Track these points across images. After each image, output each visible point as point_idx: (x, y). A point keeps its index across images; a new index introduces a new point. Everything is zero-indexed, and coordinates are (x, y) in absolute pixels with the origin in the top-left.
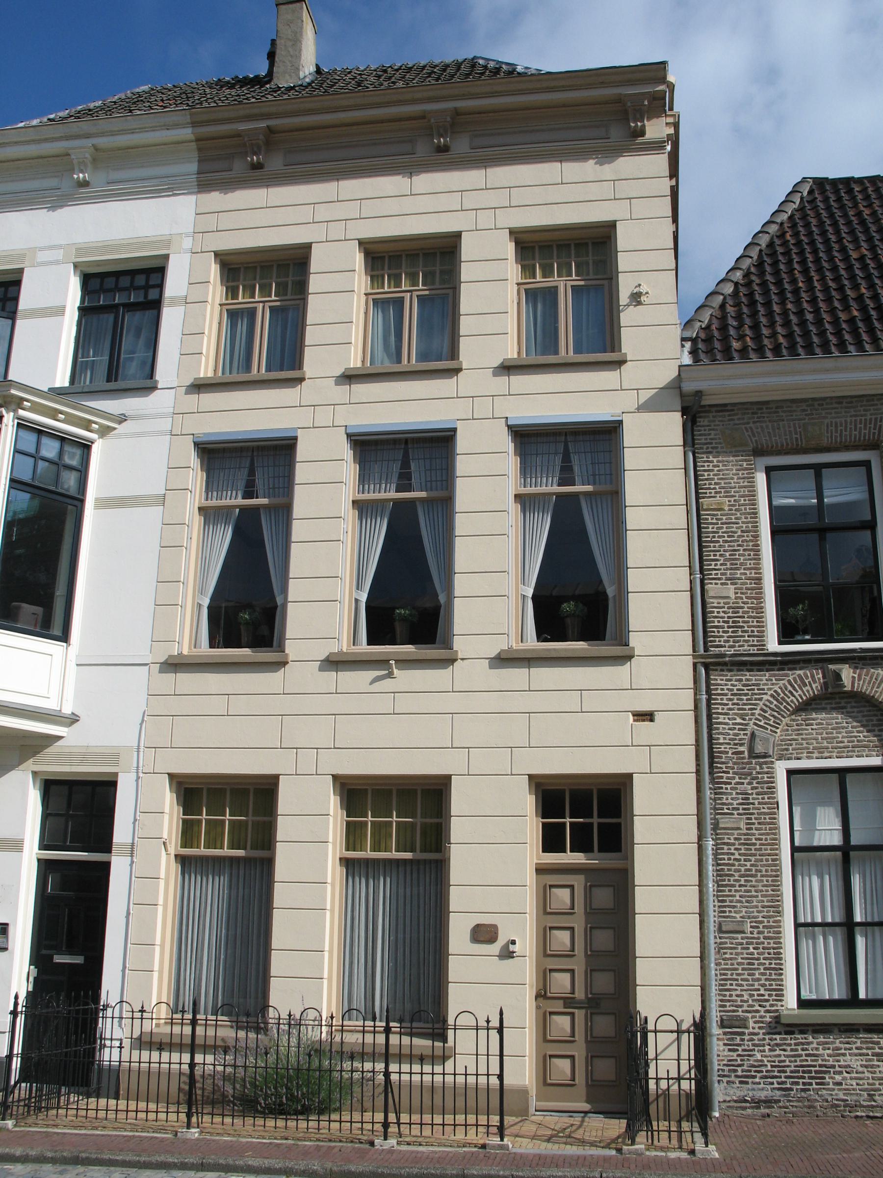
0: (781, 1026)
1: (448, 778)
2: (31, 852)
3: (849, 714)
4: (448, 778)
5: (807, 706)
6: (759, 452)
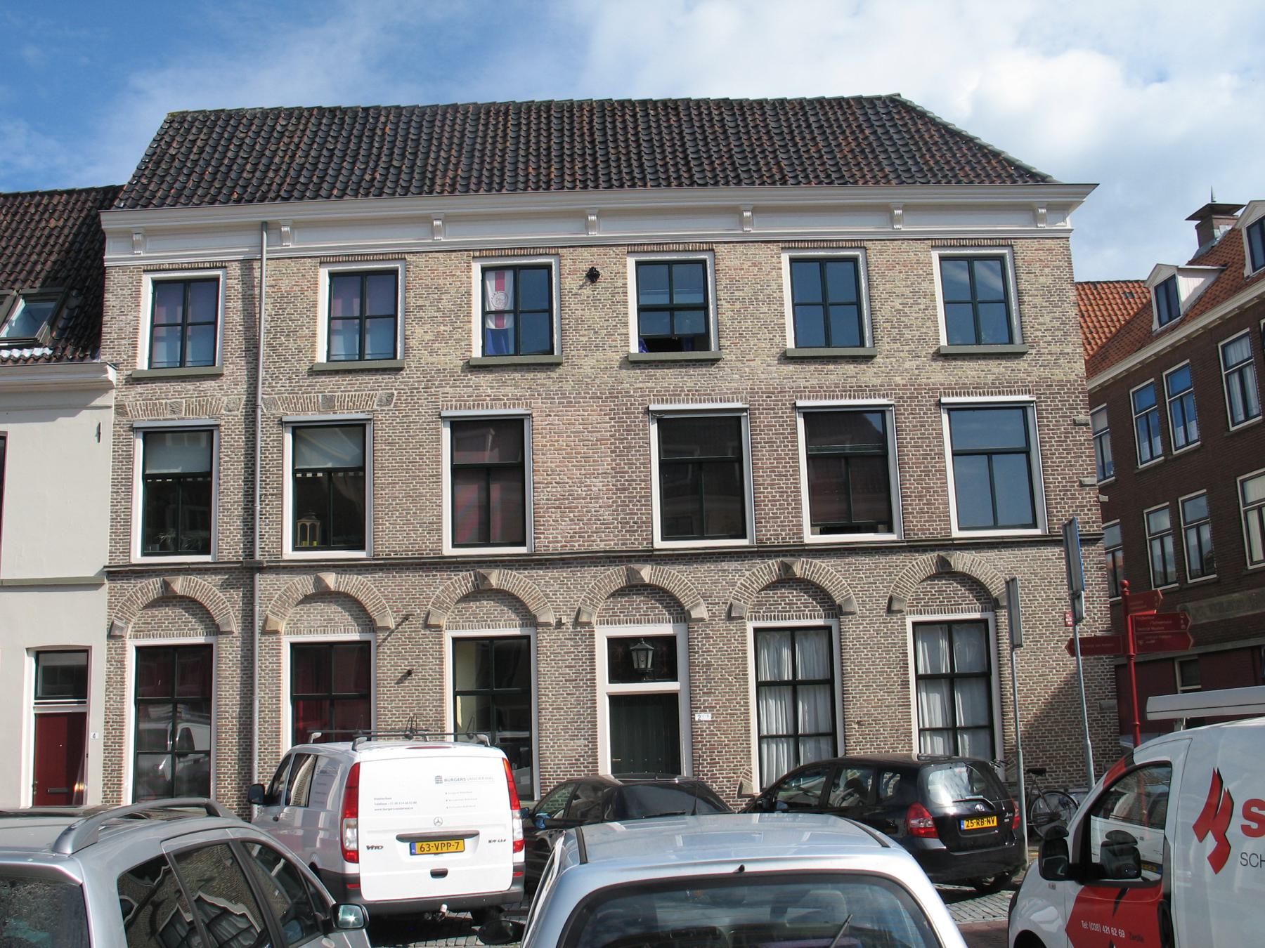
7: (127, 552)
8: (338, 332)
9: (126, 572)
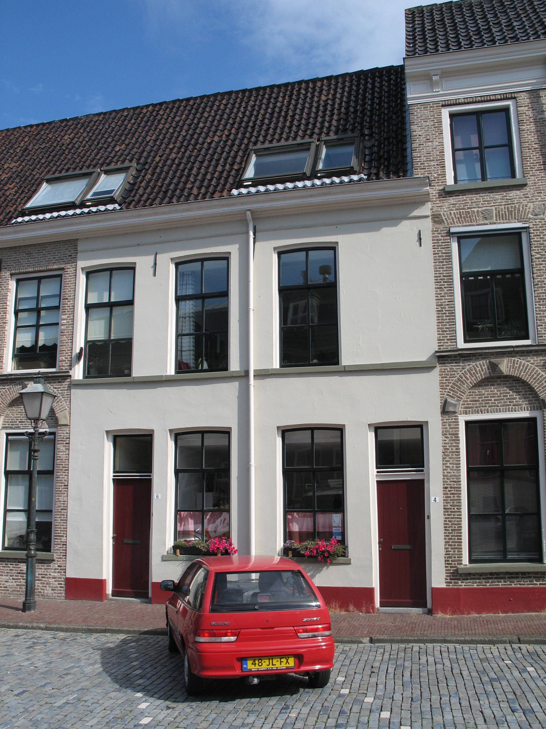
7: (454, 339)
8: (461, 162)
9: (455, 356)
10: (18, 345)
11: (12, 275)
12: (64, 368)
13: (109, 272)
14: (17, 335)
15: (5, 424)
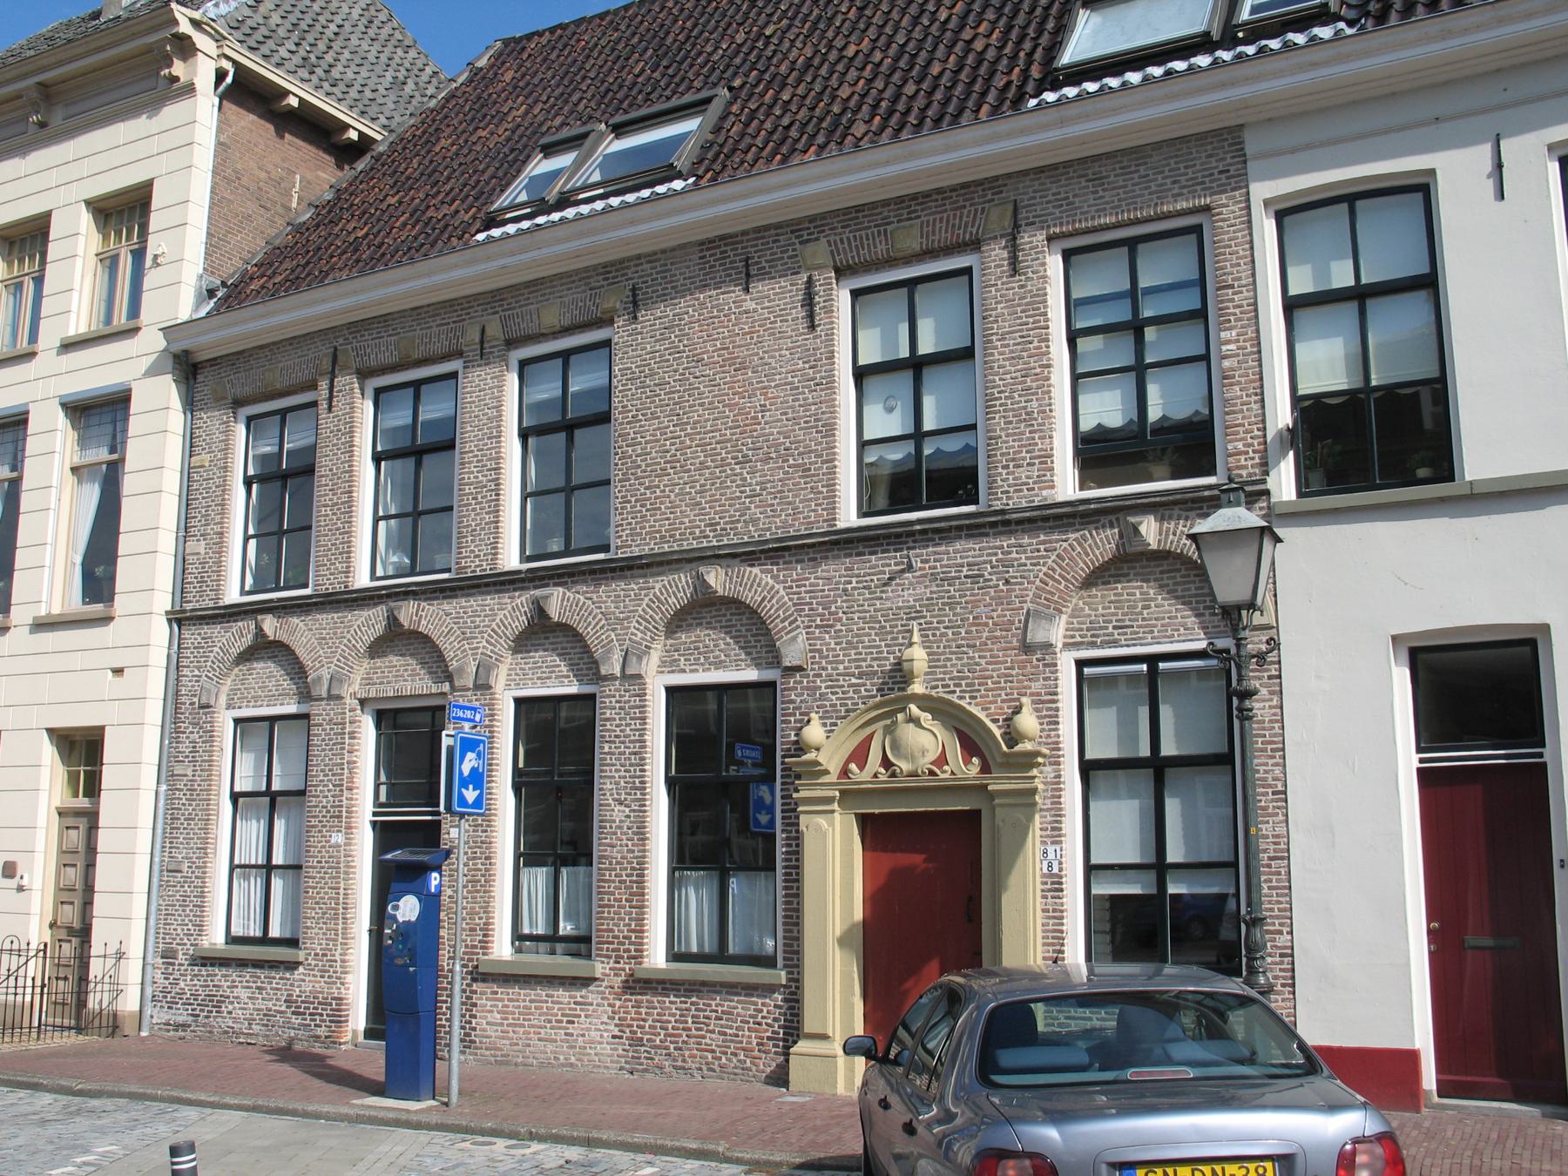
0: (207, 960)
1: (102, 728)
2: (1408, 760)
3: (709, 626)
4: (102, 728)
5: (1100, 576)
6: (238, 403)
10: (1086, 425)
11: (1050, 239)
12: (1244, 473)
13: (1344, 206)
14: (1081, 398)
15: (1073, 637)
